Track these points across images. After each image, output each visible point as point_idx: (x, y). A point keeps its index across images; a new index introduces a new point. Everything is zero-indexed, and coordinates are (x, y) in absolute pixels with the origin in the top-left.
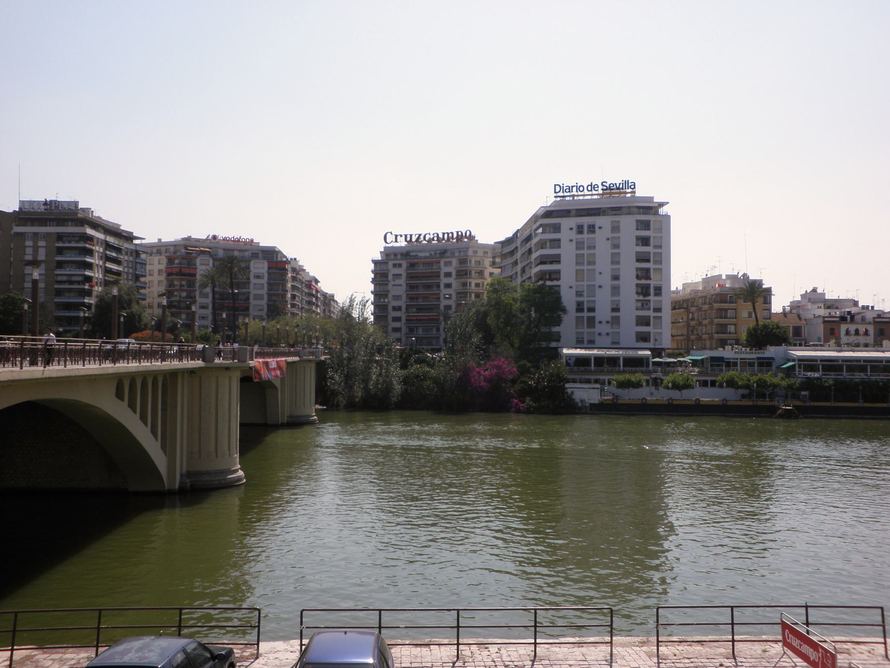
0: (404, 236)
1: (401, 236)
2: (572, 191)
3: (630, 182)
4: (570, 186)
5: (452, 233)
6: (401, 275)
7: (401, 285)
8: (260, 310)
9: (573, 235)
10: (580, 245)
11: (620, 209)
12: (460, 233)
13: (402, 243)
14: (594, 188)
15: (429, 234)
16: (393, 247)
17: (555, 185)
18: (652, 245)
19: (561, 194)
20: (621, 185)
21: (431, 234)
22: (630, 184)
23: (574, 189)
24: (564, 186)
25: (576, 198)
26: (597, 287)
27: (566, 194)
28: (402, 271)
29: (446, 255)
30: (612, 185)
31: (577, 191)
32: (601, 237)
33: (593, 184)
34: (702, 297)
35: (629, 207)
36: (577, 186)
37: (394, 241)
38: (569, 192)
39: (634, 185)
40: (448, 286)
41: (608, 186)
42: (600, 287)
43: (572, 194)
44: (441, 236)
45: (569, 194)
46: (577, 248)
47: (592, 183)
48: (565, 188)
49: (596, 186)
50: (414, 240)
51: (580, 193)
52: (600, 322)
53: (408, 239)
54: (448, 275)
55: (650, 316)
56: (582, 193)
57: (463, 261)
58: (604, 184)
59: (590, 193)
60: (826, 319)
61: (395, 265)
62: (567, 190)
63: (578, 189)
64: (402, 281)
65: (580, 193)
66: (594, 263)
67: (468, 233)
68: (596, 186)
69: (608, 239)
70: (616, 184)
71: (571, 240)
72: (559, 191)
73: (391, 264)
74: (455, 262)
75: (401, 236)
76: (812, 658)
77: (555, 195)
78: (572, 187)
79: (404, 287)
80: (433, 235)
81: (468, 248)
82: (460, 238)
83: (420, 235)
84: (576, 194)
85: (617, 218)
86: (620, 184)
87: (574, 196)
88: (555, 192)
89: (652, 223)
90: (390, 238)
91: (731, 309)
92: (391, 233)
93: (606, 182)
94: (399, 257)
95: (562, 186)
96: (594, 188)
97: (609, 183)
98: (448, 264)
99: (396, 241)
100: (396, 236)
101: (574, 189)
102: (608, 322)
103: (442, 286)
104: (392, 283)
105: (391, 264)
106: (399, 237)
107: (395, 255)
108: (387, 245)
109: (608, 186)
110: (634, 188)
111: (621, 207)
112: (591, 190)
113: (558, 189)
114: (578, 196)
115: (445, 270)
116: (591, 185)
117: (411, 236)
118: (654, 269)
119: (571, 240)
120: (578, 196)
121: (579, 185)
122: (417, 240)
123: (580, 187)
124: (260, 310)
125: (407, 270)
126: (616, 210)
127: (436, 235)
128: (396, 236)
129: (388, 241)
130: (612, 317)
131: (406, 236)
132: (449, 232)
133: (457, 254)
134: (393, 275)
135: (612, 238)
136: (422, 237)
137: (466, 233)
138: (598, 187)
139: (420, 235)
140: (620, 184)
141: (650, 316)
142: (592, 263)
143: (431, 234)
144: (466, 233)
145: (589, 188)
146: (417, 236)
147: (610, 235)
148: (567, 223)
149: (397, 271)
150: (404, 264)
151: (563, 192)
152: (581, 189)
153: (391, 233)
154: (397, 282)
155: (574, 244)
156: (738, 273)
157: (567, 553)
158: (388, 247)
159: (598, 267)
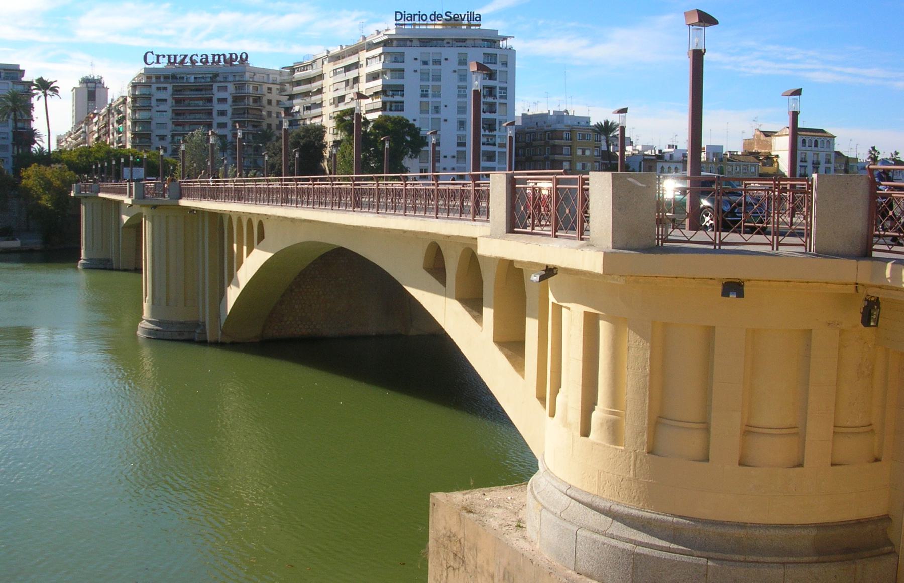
0: (167, 57)
1: (164, 56)
2: (414, 20)
3: (475, 13)
4: (412, 14)
5: (224, 55)
6: (165, 100)
7: (166, 112)
8: (3, 138)
9: (418, 65)
10: (424, 76)
11: (464, 40)
12: (234, 56)
13: (164, 63)
14: (438, 17)
15: (197, 55)
16: (154, 69)
17: (396, 12)
18: (498, 79)
19: (402, 22)
20: (466, 16)
21: (199, 56)
22: (475, 16)
23: (417, 17)
24: (406, 13)
25: (417, 27)
26: (442, 120)
27: (407, 22)
28: (167, 95)
29: (218, 79)
30: (456, 16)
31: (419, 20)
32: (448, 70)
33: (437, 13)
34: (530, 133)
35: (475, 39)
36: (419, 15)
37: (155, 61)
38: (411, 20)
39: (480, 17)
40: (222, 113)
41: (452, 16)
42: (446, 120)
43: (413, 22)
44: (228, 56)
45: (410, 22)
46: (422, 80)
47: (435, 12)
48: (406, 16)
49: (440, 16)
50: (178, 60)
51: (422, 22)
52: (446, 157)
53: (172, 61)
54: (222, 101)
55: (495, 151)
56: (425, 22)
57: (240, 86)
58: (448, 14)
59: (434, 22)
60: (646, 157)
61: (158, 89)
62: (478, 19)
63: (421, 18)
64: (168, 107)
65: (422, 22)
66: (440, 96)
67: (244, 56)
68: (440, 16)
69: (455, 71)
70: (460, 15)
71: (416, 71)
72: (401, 19)
73: (154, 87)
74: (231, 88)
75: (164, 56)
76: (197, 339)
77: (396, 22)
78: (415, 15)
79: (170, 114)
80: (202, 56)
81: (245, 72)
82: (230, 61)
83: (186, 56)
84: (418, 22)
85: (462, 50)
86: (465, 15)
87: (415, 24)
88: (396, 20)
89: (498, 56)
90: (151, 58)
91: (566, 146)
92: (152, 52)
93: (451, 12)
94: (162, 80)
95: (403, 13)
96: (438, 17)
97: (453, 13)
98: (225, 89)
99: (158, 62)
100: (158, 56)
101: (417, 17)
102: (453, 157)
103: (215, 114)
104: (155, 109)
105: (154, 87)
106: (161, 58)
107: (158, 78)
108: (147, 66)
109: (452, 16)
110: (480, 20)
111: (466, 39)
112: (435, 20)
113: (399, 16)
114: (419, 25)
115: (217, 95)
116: (435, 15)
117: (175, 56)
118: (499, 104)
119: (416, 71)
120: (419, 25)
121: (421, 13)
122: (182, 62)
123: (423, 15)
124: (3, 138)
125: (173, 95)
126: (461, 41)
127: (204, 56)
128: (158, 56)
129: (149, 61)
130: (683, 160)
131: (169, 56)
132: (221, 54)
133: (230, 78)
134: (158, 100)
135: (458, 70)
136: (188, 60)
137: (241, 56)
138: (442, 16)
139: (186, 56)
140: (465, 15)
141: (495, 151)
142: (437, 95)
143: (199, 56)
144: (241, 56)
145: (433, 17)
146: (183, 57)
147: (456, 67)
148: (411, 53)
149: (222, 95)
150: (170, 87)
151: (405, 20)
152: (424, 17)
153: (152, 52)
154: (162, 107)
155: (419, 73)
156: (549, 111)
157: (644, 185)
158: (149, 68)
159: (443, 101)
